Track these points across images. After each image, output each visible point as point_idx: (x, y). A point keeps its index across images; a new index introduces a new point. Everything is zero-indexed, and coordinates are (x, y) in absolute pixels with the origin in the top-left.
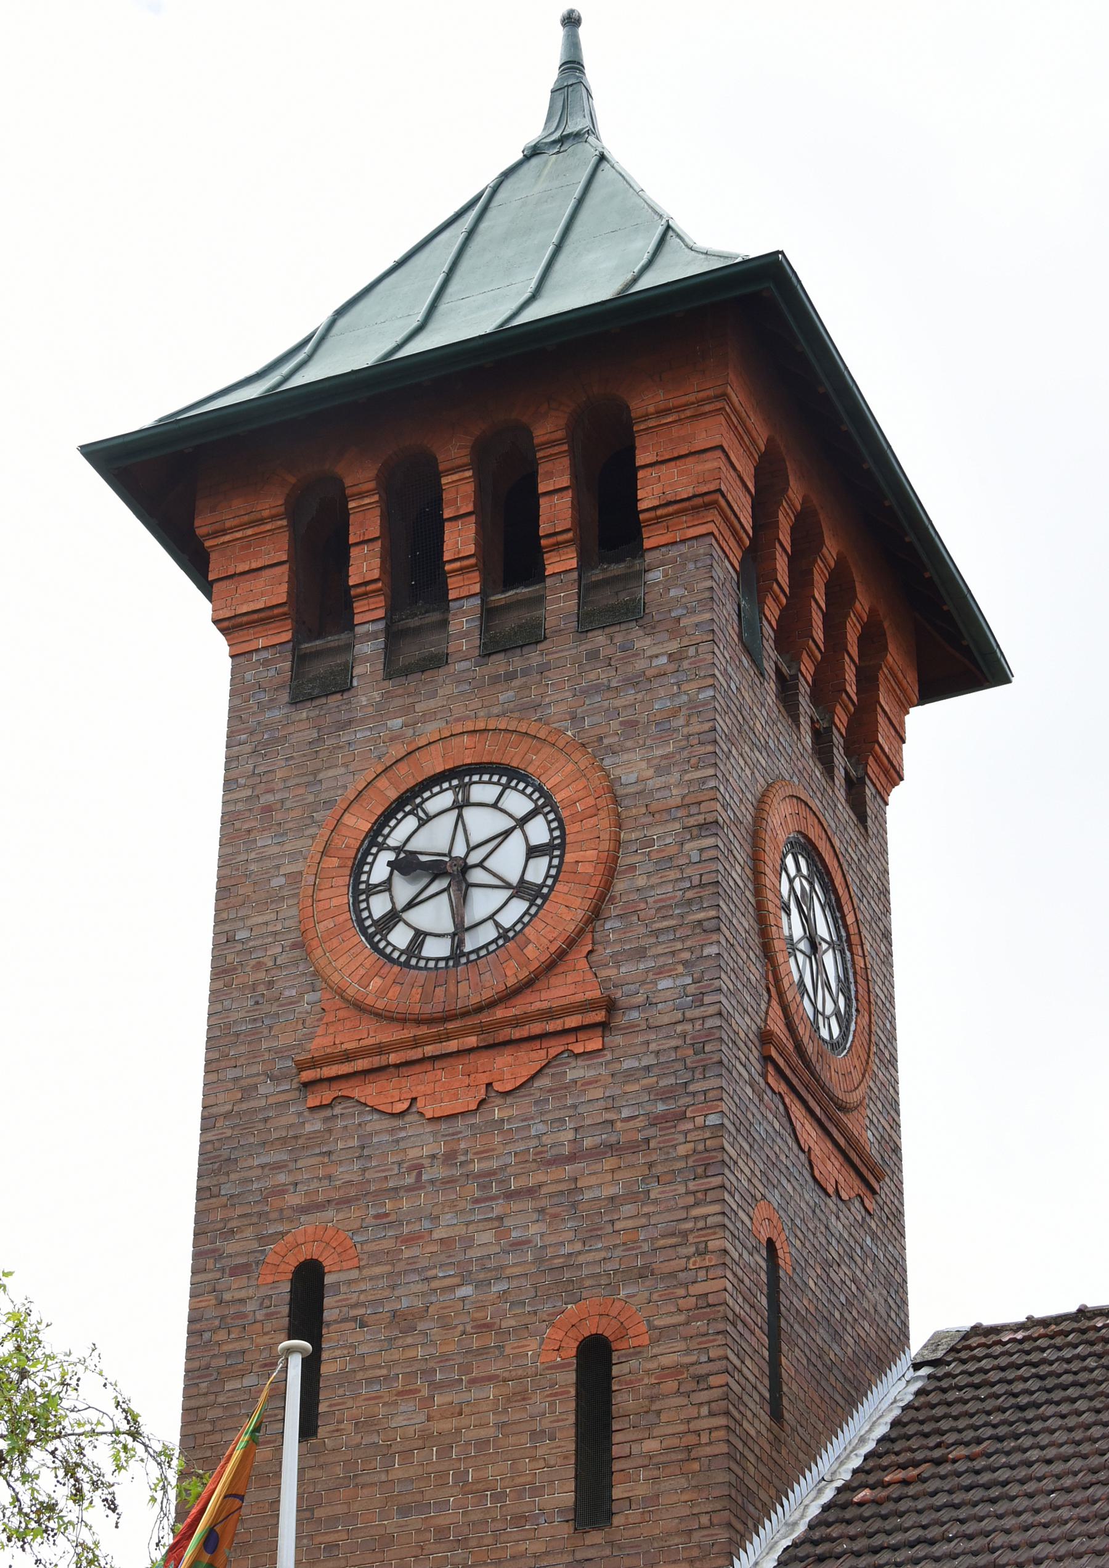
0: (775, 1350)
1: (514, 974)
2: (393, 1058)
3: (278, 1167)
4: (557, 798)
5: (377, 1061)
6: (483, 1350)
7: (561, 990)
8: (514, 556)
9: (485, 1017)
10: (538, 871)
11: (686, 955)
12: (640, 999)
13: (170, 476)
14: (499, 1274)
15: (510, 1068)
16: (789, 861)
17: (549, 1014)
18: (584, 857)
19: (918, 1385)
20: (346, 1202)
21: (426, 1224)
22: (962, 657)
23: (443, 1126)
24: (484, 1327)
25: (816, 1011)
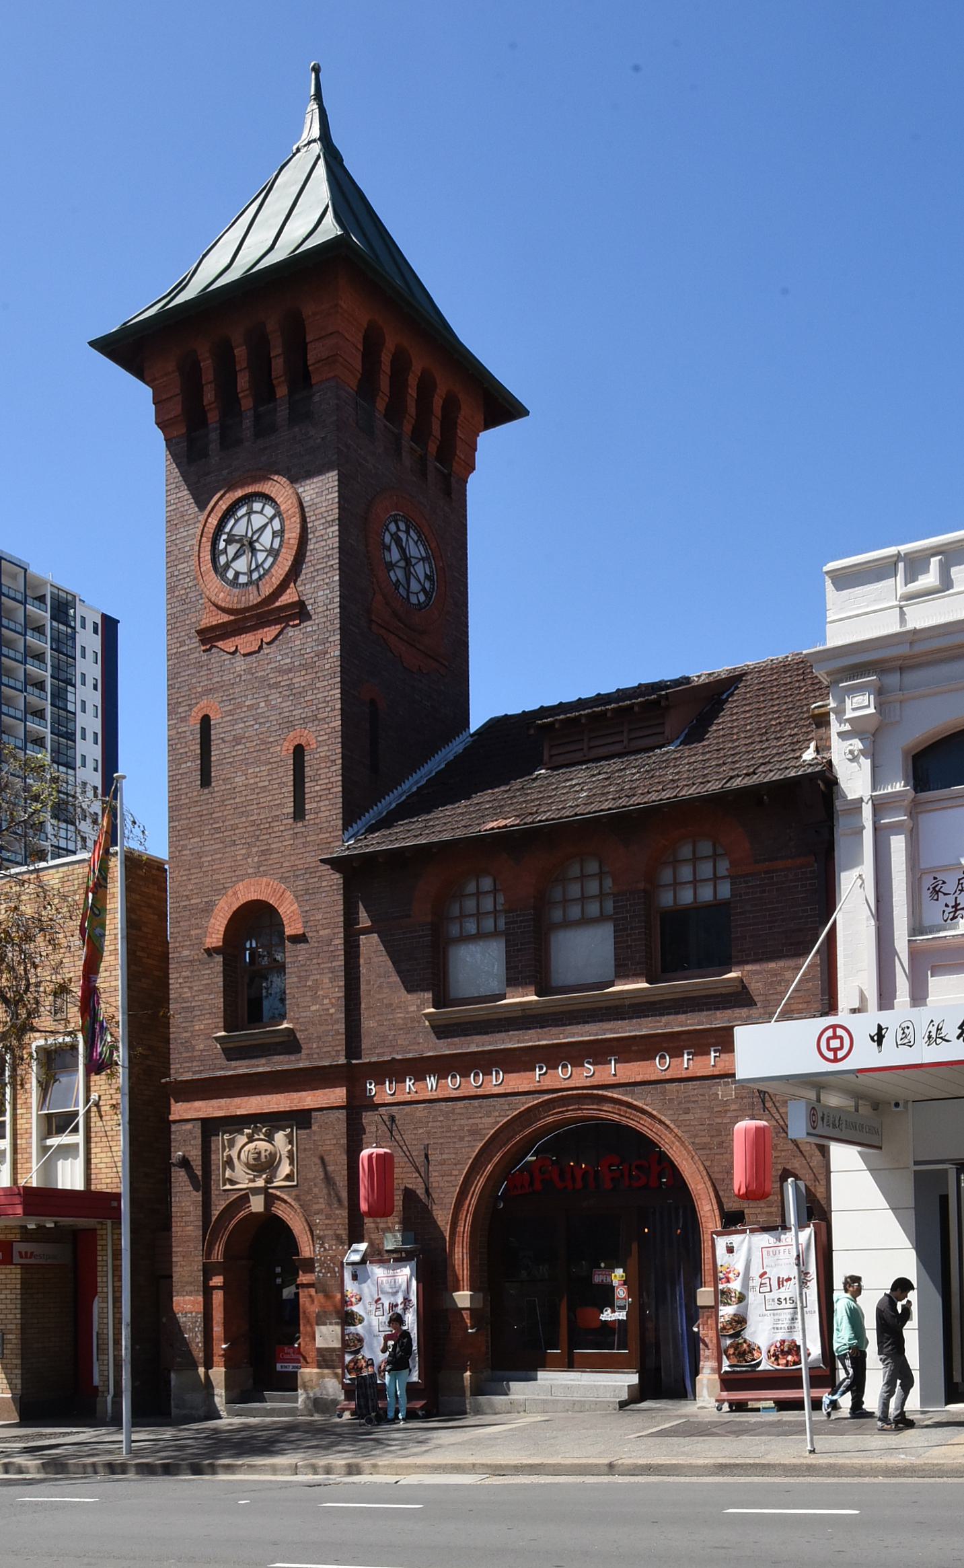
8: (264, 391)
13: (128, 348)
15: (270, 632)
18: (292, 535)
22: (502, 407)
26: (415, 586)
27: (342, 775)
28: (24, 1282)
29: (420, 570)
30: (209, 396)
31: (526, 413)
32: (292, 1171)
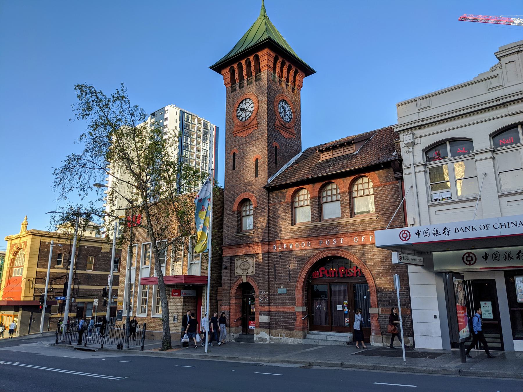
18: (256, 108)
26: (287, 117)
28: (184, 301)
29: (288, 113)
30: (237, 76)
31: (314, 72)
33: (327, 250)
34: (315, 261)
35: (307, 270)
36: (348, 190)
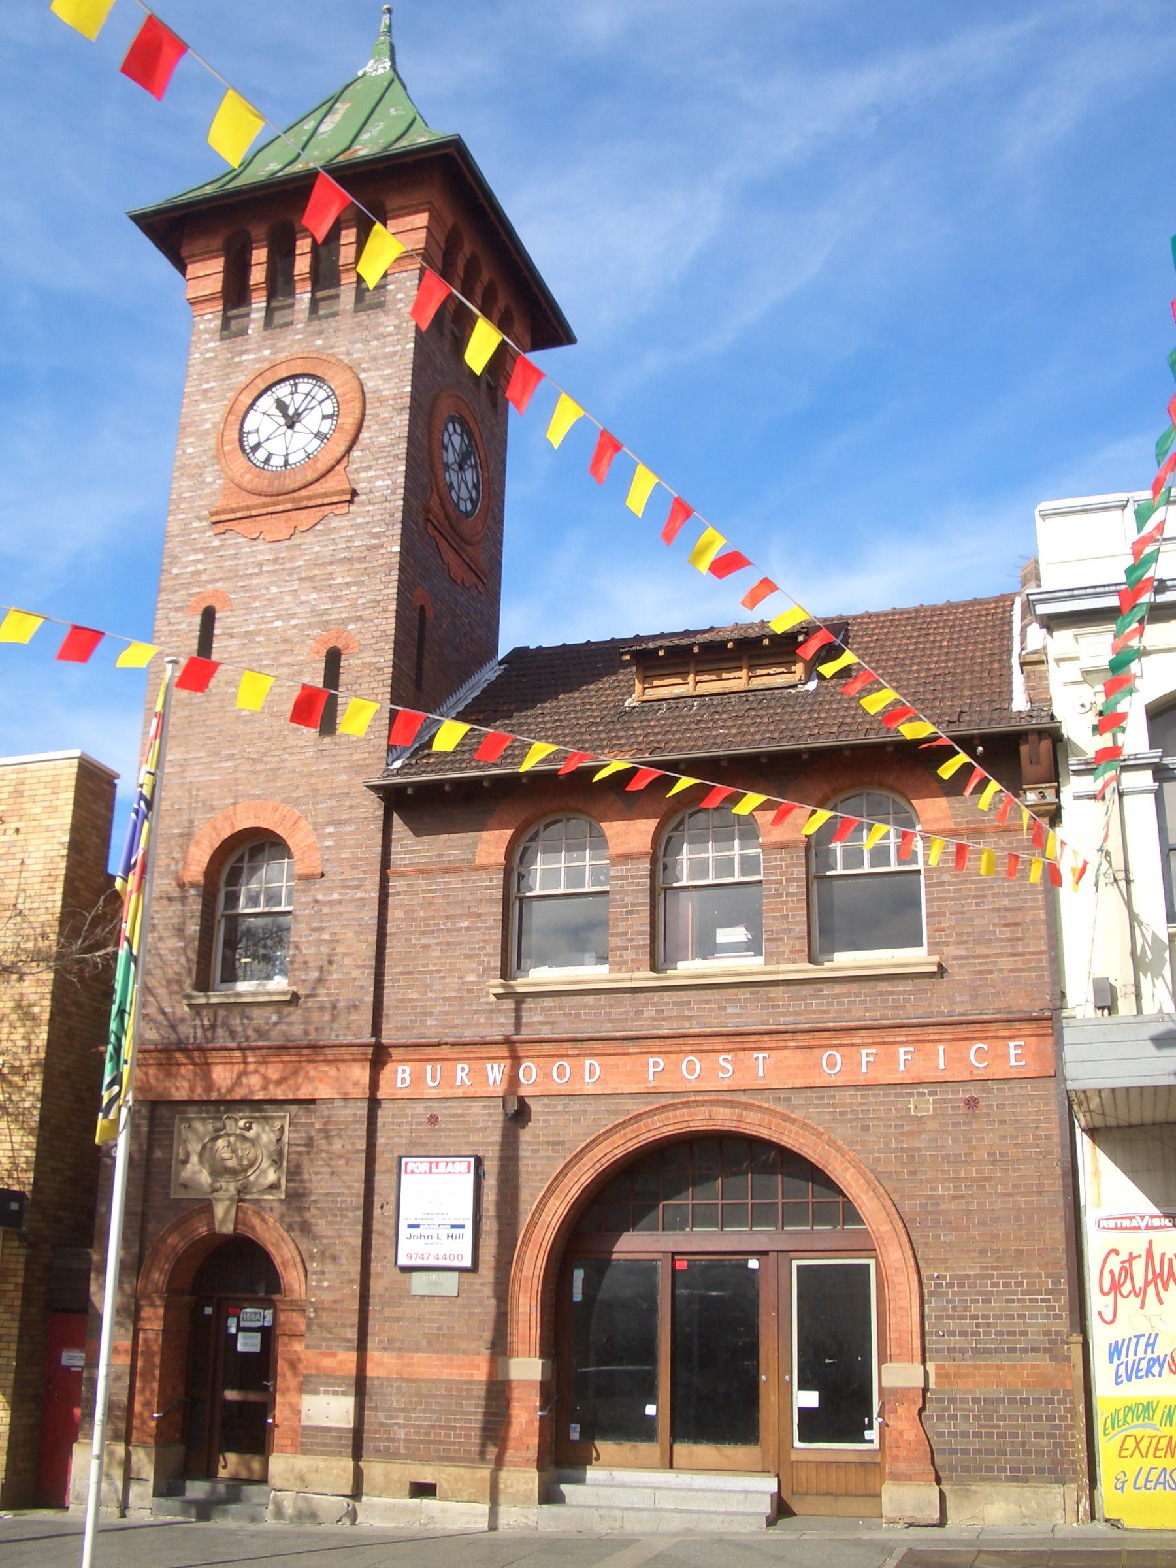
0: (420, 656)
1: (311, 476)
2: (254, 513)
3: (199, 561)
4: (337, 392)
5: (246, 513)
6: (284, 651)
7: (332, 483)
9: (296, 495)
10: (326, 426)
11: (390, 471)
12: (367, 490)
14: (293, 616)
16: (450, 427)
17: (325, 495)
19: (499, 673)
20: (228, 579)
21: (264, 591)
23: (274, 545)
24: (285, 641)
25: (459, 498)
27: (392, 686)
32: (279, 1179)
33: (687, 1104)
34: (619, 1153)
35: (575, 1192)
36: (502, 860)
